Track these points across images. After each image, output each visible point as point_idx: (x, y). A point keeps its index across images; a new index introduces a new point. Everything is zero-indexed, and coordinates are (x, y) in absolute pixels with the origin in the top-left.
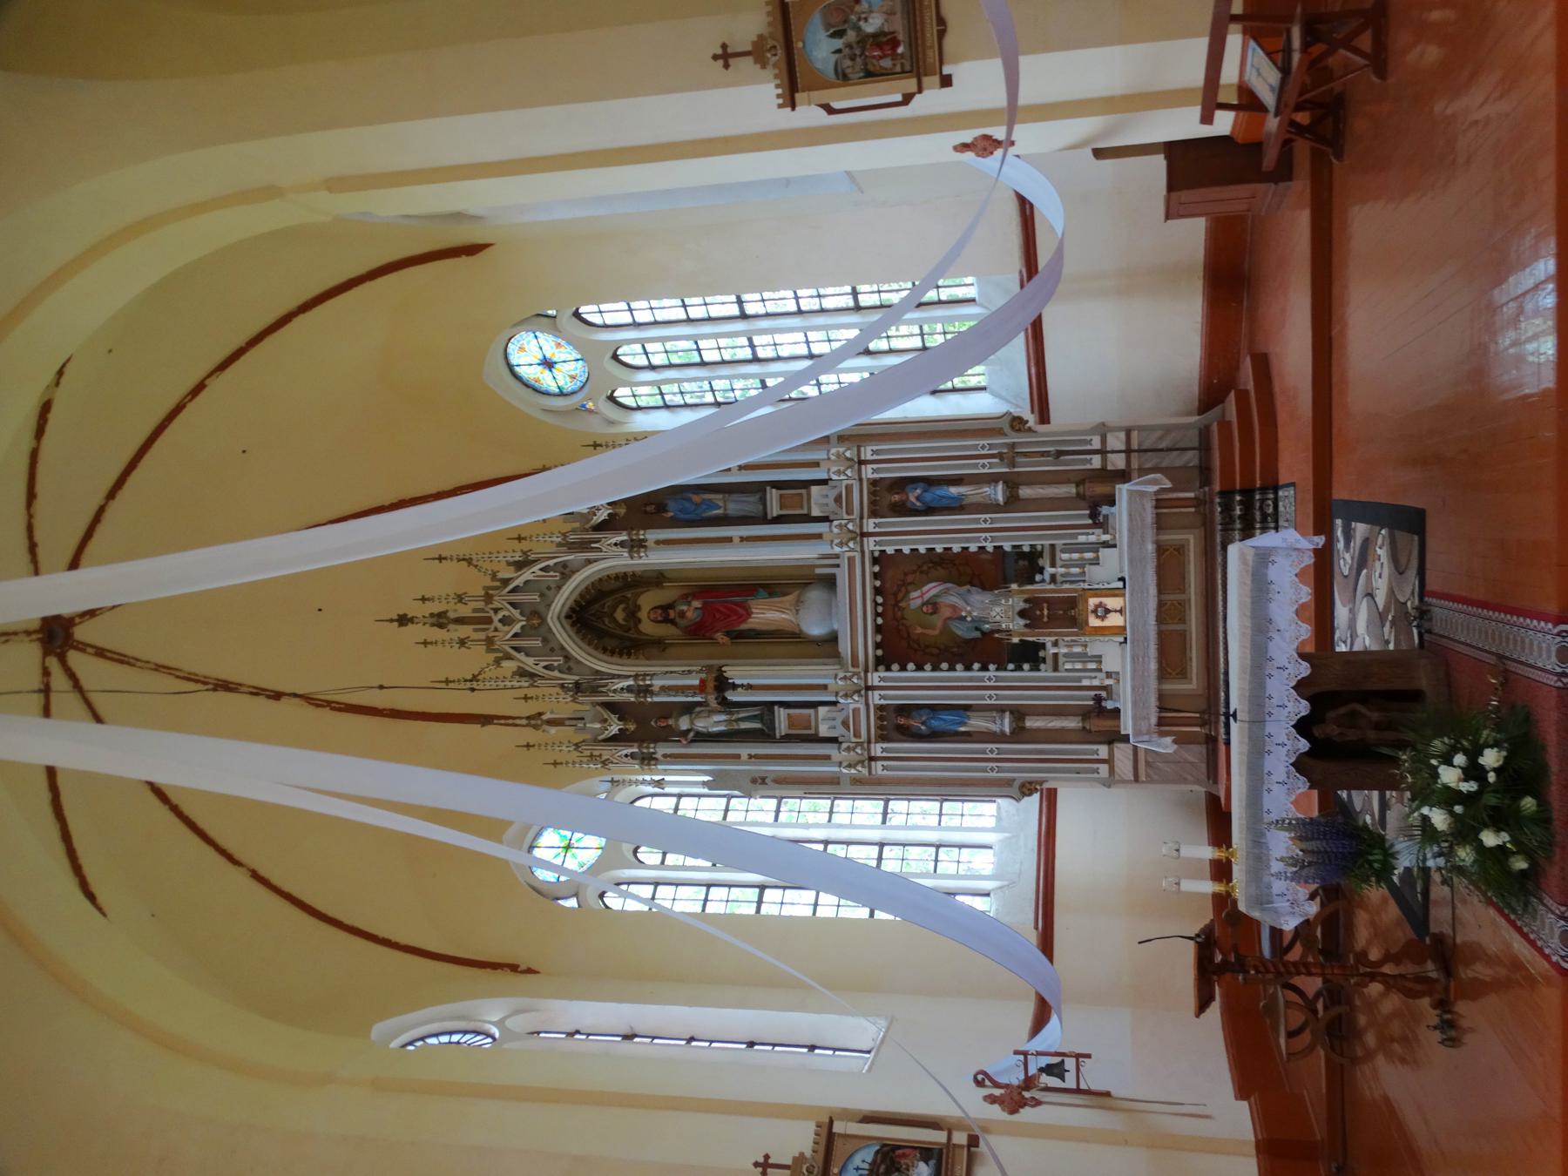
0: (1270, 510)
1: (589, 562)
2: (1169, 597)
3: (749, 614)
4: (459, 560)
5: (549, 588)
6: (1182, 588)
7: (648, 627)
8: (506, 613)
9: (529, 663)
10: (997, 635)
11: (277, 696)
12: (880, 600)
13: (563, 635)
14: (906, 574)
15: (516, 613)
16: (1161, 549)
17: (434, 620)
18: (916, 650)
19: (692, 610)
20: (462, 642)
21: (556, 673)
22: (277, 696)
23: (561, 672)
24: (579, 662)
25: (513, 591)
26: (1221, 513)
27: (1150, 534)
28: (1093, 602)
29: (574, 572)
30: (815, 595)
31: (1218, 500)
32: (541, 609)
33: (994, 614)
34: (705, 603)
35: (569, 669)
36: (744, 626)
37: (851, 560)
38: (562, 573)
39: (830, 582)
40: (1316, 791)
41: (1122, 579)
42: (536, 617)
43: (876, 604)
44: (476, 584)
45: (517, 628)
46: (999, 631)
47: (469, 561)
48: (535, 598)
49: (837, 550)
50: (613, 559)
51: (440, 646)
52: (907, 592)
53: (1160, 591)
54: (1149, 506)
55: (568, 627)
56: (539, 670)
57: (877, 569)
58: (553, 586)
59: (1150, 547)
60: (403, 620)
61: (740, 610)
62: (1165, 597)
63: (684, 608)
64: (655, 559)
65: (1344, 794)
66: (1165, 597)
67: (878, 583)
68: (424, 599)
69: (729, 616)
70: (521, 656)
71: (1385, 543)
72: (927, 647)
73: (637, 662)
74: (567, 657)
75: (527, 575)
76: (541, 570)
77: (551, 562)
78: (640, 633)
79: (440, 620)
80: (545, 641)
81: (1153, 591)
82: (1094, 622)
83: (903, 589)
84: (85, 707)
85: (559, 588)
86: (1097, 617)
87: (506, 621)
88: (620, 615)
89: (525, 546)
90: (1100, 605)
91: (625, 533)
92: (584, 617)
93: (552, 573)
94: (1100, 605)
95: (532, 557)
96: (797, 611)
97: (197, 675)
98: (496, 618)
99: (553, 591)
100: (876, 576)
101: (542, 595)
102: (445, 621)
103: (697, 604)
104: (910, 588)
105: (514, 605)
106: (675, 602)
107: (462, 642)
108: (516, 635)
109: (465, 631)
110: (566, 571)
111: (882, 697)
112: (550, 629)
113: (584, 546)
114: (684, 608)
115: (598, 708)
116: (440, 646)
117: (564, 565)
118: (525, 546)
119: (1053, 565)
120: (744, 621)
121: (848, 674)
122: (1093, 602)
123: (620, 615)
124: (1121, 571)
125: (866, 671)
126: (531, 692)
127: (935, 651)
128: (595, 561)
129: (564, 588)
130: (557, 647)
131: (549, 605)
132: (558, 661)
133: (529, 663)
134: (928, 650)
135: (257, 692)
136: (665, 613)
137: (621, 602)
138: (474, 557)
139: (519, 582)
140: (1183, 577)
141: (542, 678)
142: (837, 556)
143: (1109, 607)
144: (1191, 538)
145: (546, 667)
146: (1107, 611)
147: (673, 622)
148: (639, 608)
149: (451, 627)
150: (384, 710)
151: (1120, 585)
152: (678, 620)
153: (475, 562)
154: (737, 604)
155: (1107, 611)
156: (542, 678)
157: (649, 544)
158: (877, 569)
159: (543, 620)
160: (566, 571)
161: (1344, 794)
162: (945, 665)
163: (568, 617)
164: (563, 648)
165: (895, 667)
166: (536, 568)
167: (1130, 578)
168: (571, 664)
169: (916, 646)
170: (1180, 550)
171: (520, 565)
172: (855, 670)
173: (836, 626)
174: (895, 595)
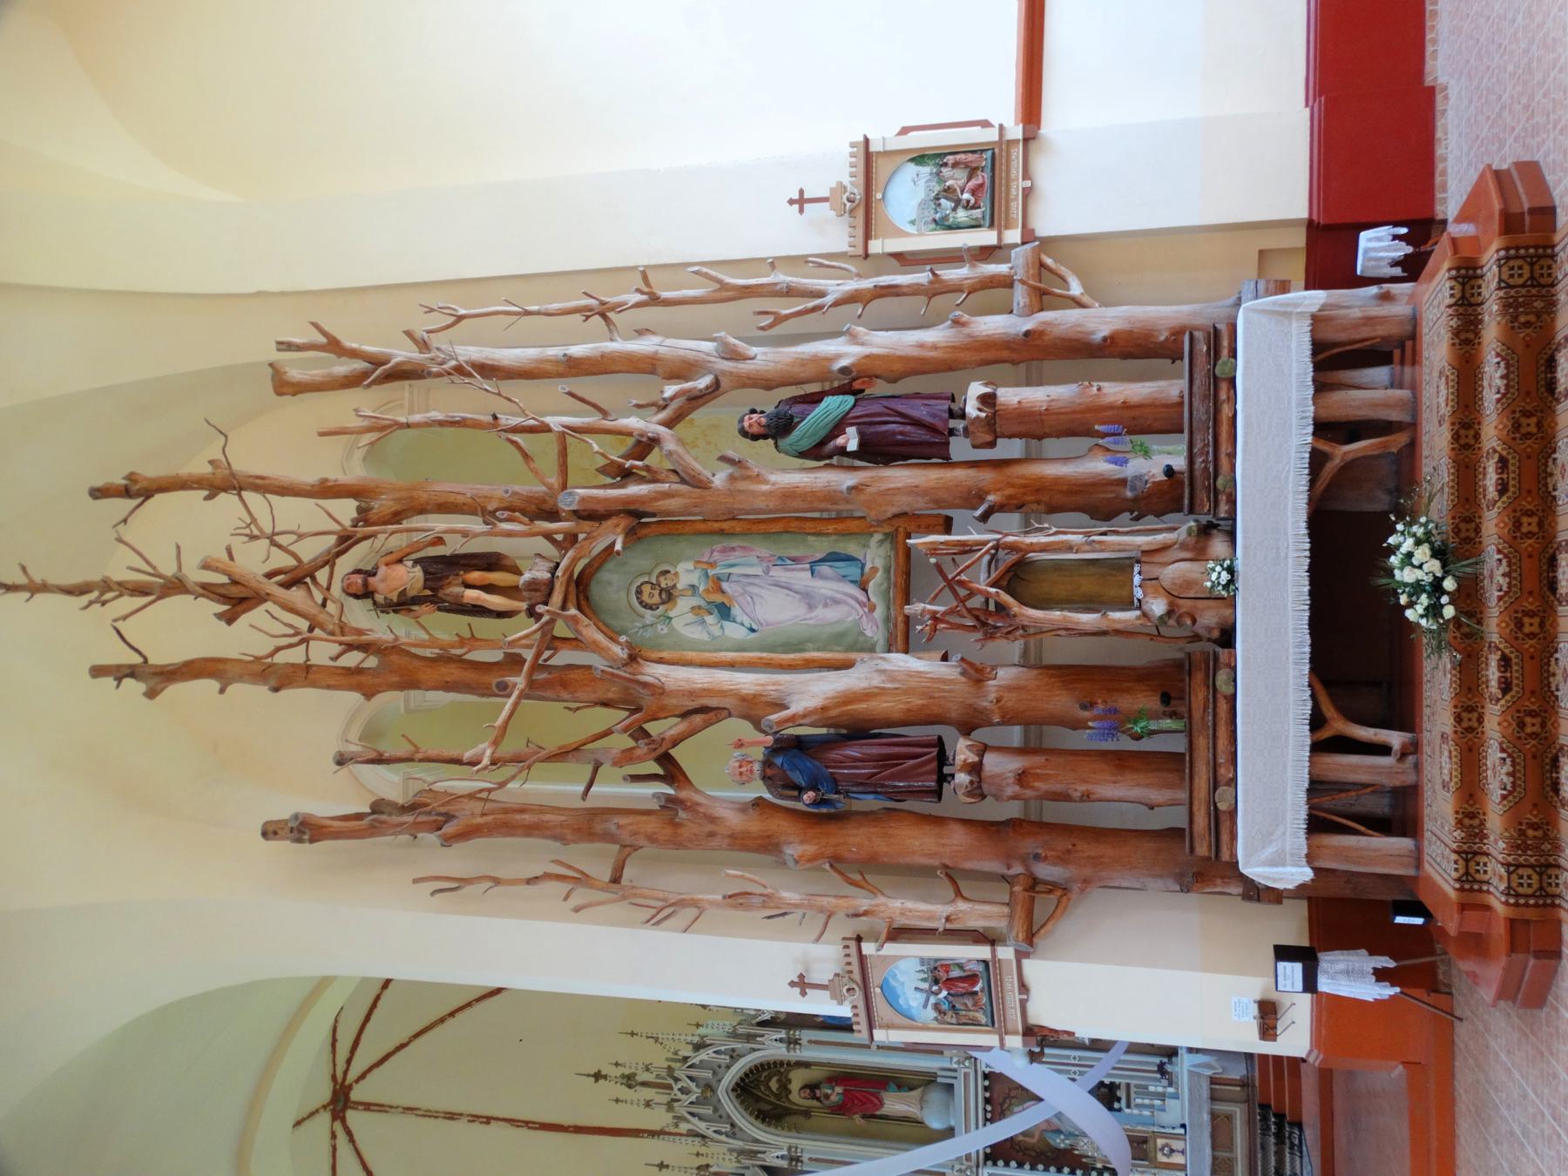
0: (1297, 1142)
1: (754, 1050)
2: (1222, 1154)
3: (882, 1104)
4: (648, 1037)
5: (720, 1067)
6: (1230, 1147)
7: (796, 1097)
8: (685, 1085)
9: (702, 1127)
10: (1084, 1160)
11: (488, 1120)
12: (989, 1108)
13: (730, 1106)
14: (1010, 1090)
15: (692, 1085)
16: (1214, 1116)
17: (625, 1081)
18: (1018, 1151)
19: (836, 1094)
20: (648, 1104)
21: (723, 1138)
22: (488, 1120)
23: (727, 1136)
24: (741, 1129)
25: (689, 1067)
26: (1260, 1120)
27: (1206, 1106)
28: (1160, 1142)
29: (740, 1056)
30: (935, 1096)
31: (1258, 1111)
32: (714, 1083)
33: (1082, 1144)
34: (845, 1090)
35: (734, 1134)
36: (878, 1113)
37: (966, 1075)
38: (731, 1057)
39: (950, 1088)
40: (1359, 273)
41: (1183, 1126)
42: (709, 1087)
43: (986, 1111)
44: (659, 1058)
45: (693, 1098)
46: (1087, 1157)
47: (656, 1040)
48: (708, 1075)
49: (955, 1066)
50: (772, 1048)
51: (629, 1104)
52: (1010, 1105)
53: (1214, 1148)
54: (1205, 1085)
55: (734, 1099)
56: (710, 1133)
57: (987, 1083)
58: (723, 1066)
59: (1206, 1117)
60: (598, 1076)
61: (875, 1100)
62: (1218, 1154)
63: (829, 1091)
64: (807, 1053)
65: (1385, 545)
66: (1218, 1154)
67: (987, 1095)
68: (617, 1064)
69: (865, 1103)
70: (695, 1120)
71: (1425, 500)
72: (1026, 1149)
73: (790, 1134)
74: (733, 1125)
75: (704, 1055)
76: (715, 1052)
77: (723, 1048)
78: (790, 1101)
79: (629, 1081)
80: (716, 1110)
81: (1208, 1151)
82: (1161, 1158)
83: (1008, 1101)
84: (354, 1152)
85: (728, 1067)
86: (1164, 1154)
87: (684, 1091)
88: (774, 1084)
89: (702, 1031)
90: (1167, 1145)
91: (784, 1031)
92: (747, 1089)
93: (723, 1057)
94: (1167, 1145)
95: (708, 1042)
96: (922, 1108)
97: (430, 1111)
98: (676, 1087)
99: (723, 1069)
100: (986, 1089)
101: (715, 1073)
102: (633, 1083)
103: (839, 1090)
104: (1013, 1101)
105: (691, 1078)
106: (821, 1083)
107: (648, 1104)
108: (692, 1103)
109: (649, 1093)
110: (734, 1056)
111: (966, 1075)
112: (720, 1100)
113: (750, 1038)
114: (829, 1091)
115: (757, 1169)
116: (629, 1104)
117: (733, 1050)
118: (702, 1031)
119: (1128, 1106)
120: (877, 1109)
121: (963, 1167)
122: (1160, 1142)
123: (774, 1084)
124: (1183, 1118)
125: (978, 1166)
126: (703, 1150)
127: (1034, 1154)
128: (759, 1050)
129: (733, 1068)
130: (725, 1116)
131: (720, 1081)
132: (726, 1128)
133: (702, 1127)
134: (1027, 1152)
135: (474, 1118)
136: (812, 1088)
137: (775, 1075)
138: (660, 1036)
139: (696, 1061)
140: (1232, 1139)
141: (712, 1140)
142: (955, 1070)
143: (1174, 1147)
144: (1238, 1110)
145: (715, 1132)
146: (1172, 1151)
147: (818, 1099)
148: (790, 1081)
149: (638, 1088)
150: (570, 1127)
151: (1182, 1131)
152: (822, 1099)
153: (660, 1040)
154: (870, 1094)
155: (1172, 1151)
156: (712, 1140)
157: (804, 1041)
158: (987, 1083)
159: (713, 1091)
160: (734, 1055)
161: (1385, 545)
162: (1041, 1167)
163: (733, 1090)
164: (729, 1117)
165: (1001, 1163)
166: (710, 1051)
167: (1190, 1125)
168: (736, 1130)
169: (1018, 1148)
170: (1229, 1118)
171: (698, 1047)
172: (969, 1164)
173: (953, 1123)
174: (1001, 1105)
